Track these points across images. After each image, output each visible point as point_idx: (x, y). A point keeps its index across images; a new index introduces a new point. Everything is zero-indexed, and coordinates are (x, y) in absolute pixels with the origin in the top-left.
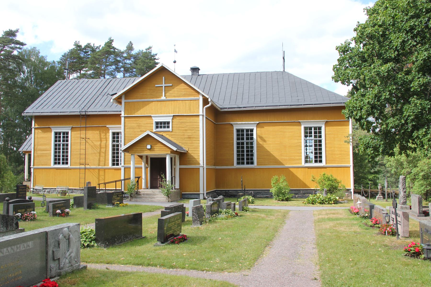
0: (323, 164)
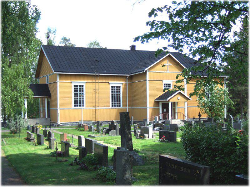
0: (85, 107)
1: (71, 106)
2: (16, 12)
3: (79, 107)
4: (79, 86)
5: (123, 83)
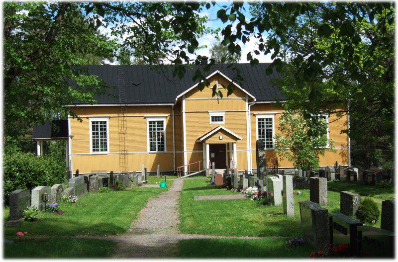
0: (108, 152)
1: (88, 151)
2: (115, 43)
3: (100, 152)
4: (265, 120)
5: (167, 117)
